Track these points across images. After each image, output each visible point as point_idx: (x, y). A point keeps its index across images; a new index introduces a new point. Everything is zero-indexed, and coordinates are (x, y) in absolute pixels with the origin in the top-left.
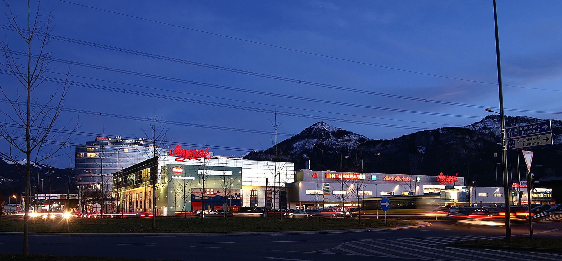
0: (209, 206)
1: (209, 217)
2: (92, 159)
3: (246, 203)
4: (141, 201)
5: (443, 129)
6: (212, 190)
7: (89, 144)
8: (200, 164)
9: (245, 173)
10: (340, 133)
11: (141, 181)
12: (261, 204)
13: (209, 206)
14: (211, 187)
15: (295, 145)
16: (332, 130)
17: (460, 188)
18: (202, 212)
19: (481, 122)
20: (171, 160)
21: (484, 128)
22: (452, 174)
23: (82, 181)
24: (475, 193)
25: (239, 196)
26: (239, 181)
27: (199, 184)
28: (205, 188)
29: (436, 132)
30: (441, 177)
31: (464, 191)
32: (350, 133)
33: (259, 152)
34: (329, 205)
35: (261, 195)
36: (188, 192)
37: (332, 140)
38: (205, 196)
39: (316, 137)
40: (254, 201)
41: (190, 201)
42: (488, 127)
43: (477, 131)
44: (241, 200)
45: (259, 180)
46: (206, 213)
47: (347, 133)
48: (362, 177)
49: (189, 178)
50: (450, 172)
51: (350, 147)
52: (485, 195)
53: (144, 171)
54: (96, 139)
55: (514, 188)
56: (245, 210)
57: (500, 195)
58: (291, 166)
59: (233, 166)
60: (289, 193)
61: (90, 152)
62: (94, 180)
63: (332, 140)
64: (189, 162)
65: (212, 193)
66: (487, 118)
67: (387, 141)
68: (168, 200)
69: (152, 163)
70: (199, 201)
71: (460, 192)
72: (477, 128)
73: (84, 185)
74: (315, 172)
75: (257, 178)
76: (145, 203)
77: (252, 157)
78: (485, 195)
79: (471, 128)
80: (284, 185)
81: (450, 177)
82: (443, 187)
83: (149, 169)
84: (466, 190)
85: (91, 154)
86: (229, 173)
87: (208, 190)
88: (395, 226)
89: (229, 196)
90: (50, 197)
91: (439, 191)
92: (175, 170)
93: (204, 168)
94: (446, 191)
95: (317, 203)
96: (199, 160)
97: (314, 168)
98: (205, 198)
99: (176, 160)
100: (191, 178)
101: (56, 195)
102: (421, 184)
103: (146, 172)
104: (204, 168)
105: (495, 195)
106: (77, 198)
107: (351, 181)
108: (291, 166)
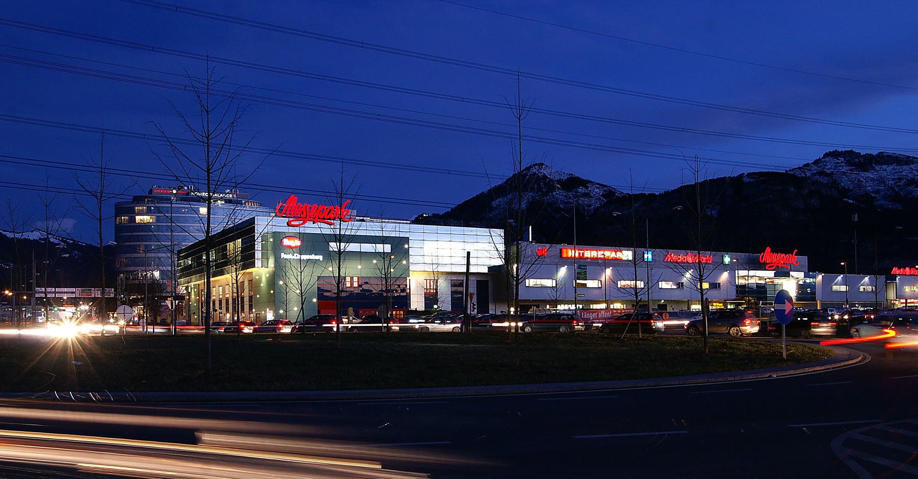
0: (351, 310)
2: (145, 227)
3: (417, 303)
4: (227, 300)
5: (749, 174)
6: (355, 279)
7: (139, 200)
8: (328, 232)
9: (414, 248)
10: (573, 183)
11: (226, 264)
13: (351, 310)
14: (354, 274)
15: (494, 204)
16: (557, 178)
17: (801, 275)
19: (817, 162)
20: (280, 224)
21: (821, 173)
22: (788, 251)
23: (127, 265)
24: (827, 283)
25: (403, 290)
26: (404, 262)
27: (330, 269)
28: (342, 274)
29: (736, 182)
30: (767, 255)
31: (808, 281)
34: (566, 307)
35: (444, 286)
36: (310, 278)
37: (559, 194)
38: (343, 291)
39: (532, 189)
40: (431, 298)
41: (315, 300)
42: (828, 171)
43: (809, 178)
45: (454, 260)
48: (627, 255)
49: (313, 257)
50: (782, 247)
51: (589, 206)
53: (230, 246)
54: (151, 192)
57: (869, 288)
59: (393, 235)
60: (496, 285)
61: (141, 213)
62: (146, 264)
63: (559, 194)
64: (311, 228)
65: (356, 285)
66: (826, 155)
68: (275, 297)
69: (246, 230)
70: (333, 300)
71: (801, 283)
72: (808, 174)
73: (131, 272)
74: (539, 246)
75: (445, 255)
76: (234, 303)
79: (798, 173)
81: (783, 255)
82: (771, 274)
85: (142, 217)
86: (388, 248)
87: (348, 279)
92: (286, 242)
93: (339, 238)
94: (777, 281)
95: (545, 302)
96: (330, 224)
97: (537, 239)
98: (343, 294)
99: (289, 224)
100: (317, 257)
102: (732, 268)
103: (235, 246)
104: (339, 238)
105: (861, 289)
106: (112, 296)
107: (606, 263)
108: (498, 235)
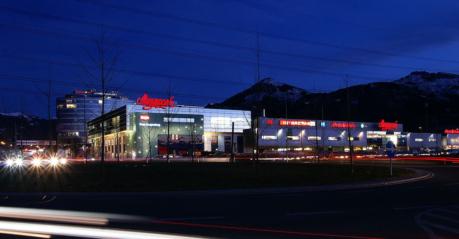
0: (174, 151)
1: (175, 164)
2: (71, 110)
3: (207, 148)
4: (113, 146)
6: (177, 136)
7: (68, 97)
9: (206, 120)
10: (285, 88)
11: (113, 128)
13: (174, 151)
14: (176, 133)
15: (247, 98)
19: (407, 77)
20: (139, 108)
22: (392, 121)
24: (412, 138)
25: (201, 141)
27: (164, 131)
28: (170, 134)
30: (383, 124)
31: (403, 136)
34: (282, 150)
35: (221, 139)
36: (154, 135)
37: (278, 93)
38: (170, 142)
40: (214, 145)
41: (156, 146)
42: (413, 82)
44: (203, 145)
46: (171, 156)
47: (291, 88)
48: (312, 124)
49: (155, 125)
51: (294, 99)
52: (420, 140)
53: (114, 119)
54: (74, 92)
55: (446, 134)
56: (206, 154)
57: (434, 140)
60: (247, 138)
63: (278, 93)
65: (177, 139)
66: (412, 74)
68: (137, 145)
69: (122, 112)
70: (165, 146)
75: (221, 124)
76: (116, 148)
78: (420, 140)
79: (398, 83)
80: (242, 132)
82: (384, 133)
87: (173, 136)
89: (193, 142)
92: (142, 117)
93: (168, 116)
94: (388, 136)
95: (272, 147)
98: (171, 143)
102: (365, 130)
104: (168, 116)
105: (430, 140)
107: (302, 127)
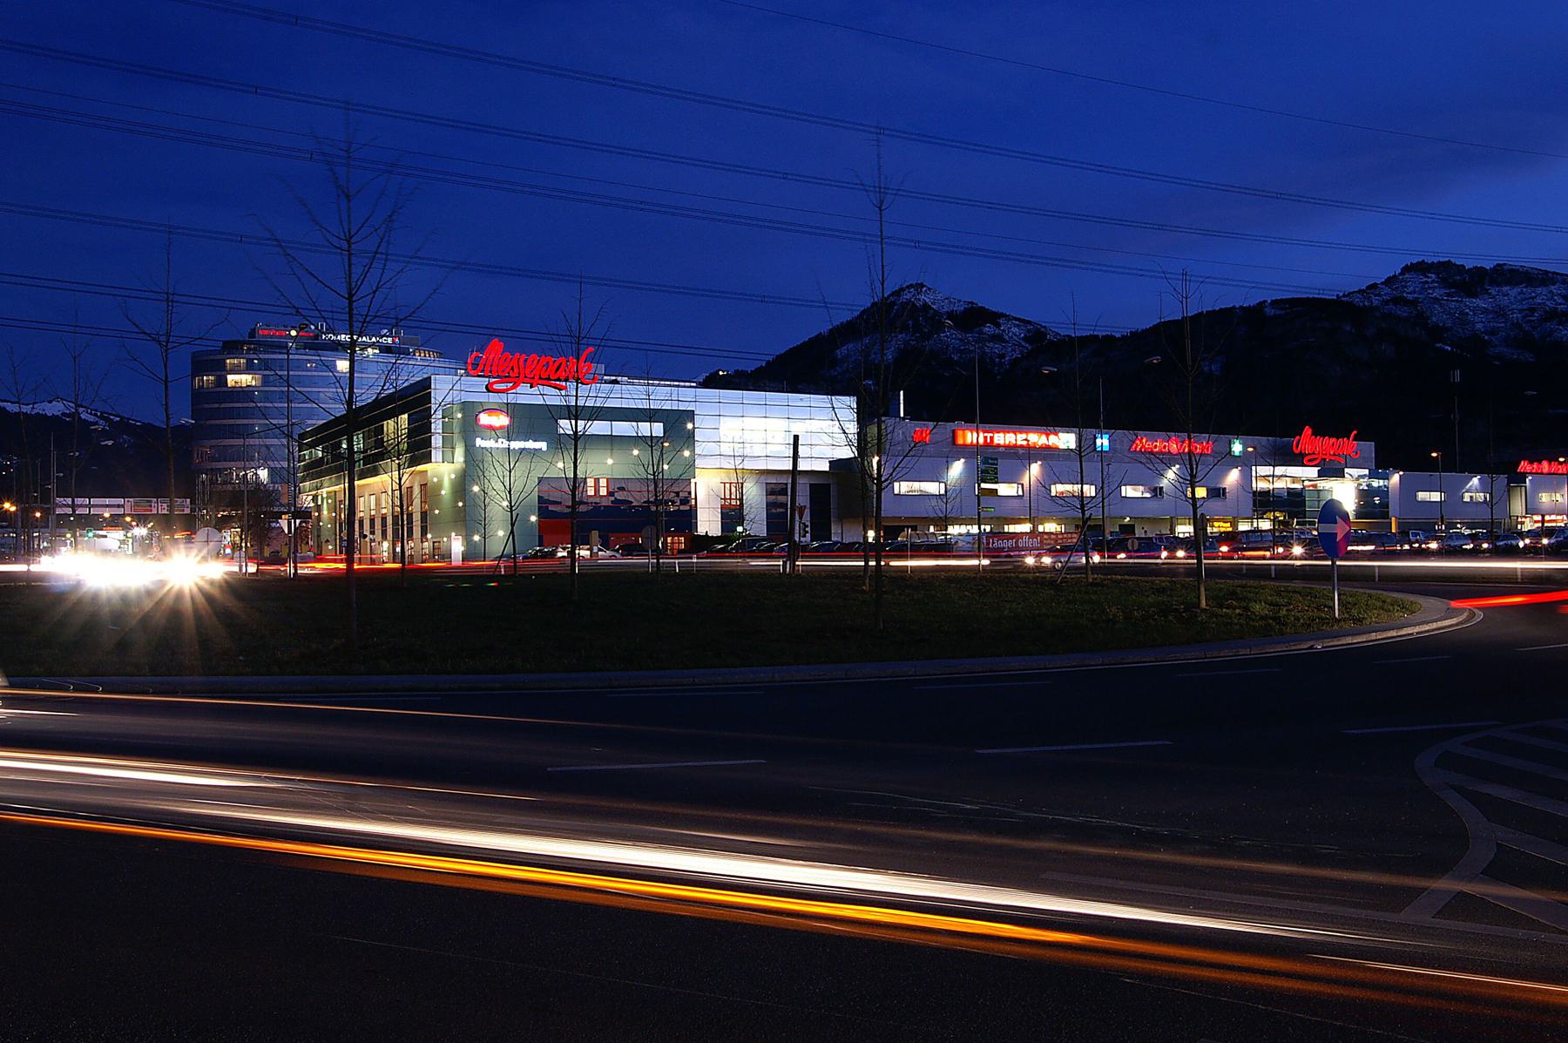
0: (595, 534)
2: (243, 393)
3: (708, 523)
4: (384, 519)
5: (1275, 303)
6: (603, 482)
7: (232, 348)
8: (556, 401)
9: (702, 429)
10: (974, 317)
11: (381, 456)
12: (756, 524)
13: (595, 534)
14: (601, 472)
15: (841, 352)
18: (572, 553)
19: (1389, 281)
20: (474, 388)
21: (1397, 301)
24: (1407, 489)
25: (686, 501)
26: (687, 453)
27: (560, 465)
28: (580, 475)
30: (1306, 440)
32: (1002, 315)
33: (736, 371)
35: (754, 494)
37: (950, 336)
38: (582, 503)
40: (732, 515)
41: (533, 518)
42: (1410, 297)
45: (771, 450)
46: (585, 553)
47: (994, 317)
49: (530, 444)
51: (1002, 356)
52: (1435, 497)
53: (389, 426)
54: (252, 333)
56: (703, 544)
58: (846, 406)
60: (843, 492)
63: (950, 336)
64: (528, 395)
65: (603, 492)
66: (1406, 269)
67: (1109, 339)
68: (467, 515)
69: (415, 400)
70: (564, 515)
72: (1376, 301)
75: (753, 441)
76: (395, 523)
77: (712, 382)
78: (1435, 497)
79: (1357, 300)
82: (1312, 472)
83: (405, 416)
84: (1382, 482)
87: (590, 482)
88: (905, 557)
89: (657, 502)
90: (90, 506)
91: (1298, 486)
92: (485, 419)
93: (575, 413)
98: (582, 508)
99: (489, 389)
101: (121, 501)
102: (1245, 462)
103: (397, 427)
104: (575, 413)
105: (1467, 498)
108: (846, 406)
